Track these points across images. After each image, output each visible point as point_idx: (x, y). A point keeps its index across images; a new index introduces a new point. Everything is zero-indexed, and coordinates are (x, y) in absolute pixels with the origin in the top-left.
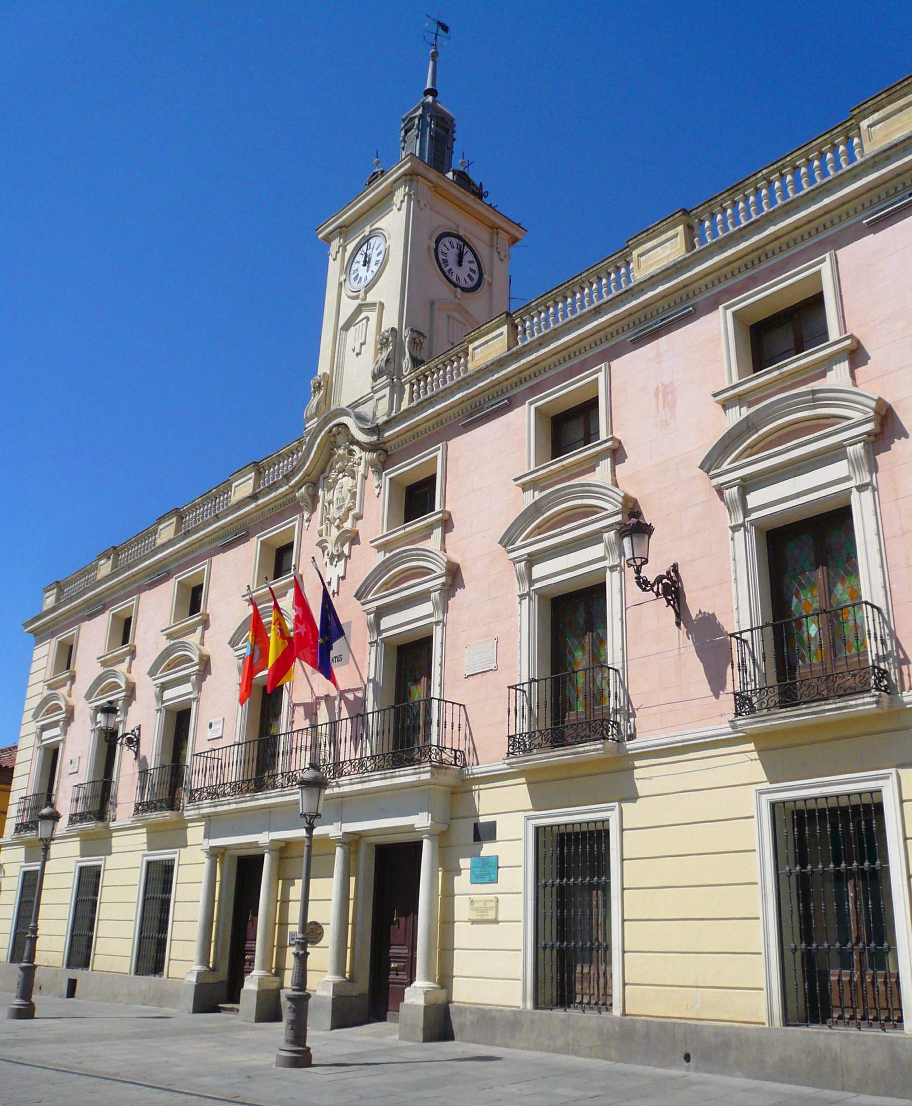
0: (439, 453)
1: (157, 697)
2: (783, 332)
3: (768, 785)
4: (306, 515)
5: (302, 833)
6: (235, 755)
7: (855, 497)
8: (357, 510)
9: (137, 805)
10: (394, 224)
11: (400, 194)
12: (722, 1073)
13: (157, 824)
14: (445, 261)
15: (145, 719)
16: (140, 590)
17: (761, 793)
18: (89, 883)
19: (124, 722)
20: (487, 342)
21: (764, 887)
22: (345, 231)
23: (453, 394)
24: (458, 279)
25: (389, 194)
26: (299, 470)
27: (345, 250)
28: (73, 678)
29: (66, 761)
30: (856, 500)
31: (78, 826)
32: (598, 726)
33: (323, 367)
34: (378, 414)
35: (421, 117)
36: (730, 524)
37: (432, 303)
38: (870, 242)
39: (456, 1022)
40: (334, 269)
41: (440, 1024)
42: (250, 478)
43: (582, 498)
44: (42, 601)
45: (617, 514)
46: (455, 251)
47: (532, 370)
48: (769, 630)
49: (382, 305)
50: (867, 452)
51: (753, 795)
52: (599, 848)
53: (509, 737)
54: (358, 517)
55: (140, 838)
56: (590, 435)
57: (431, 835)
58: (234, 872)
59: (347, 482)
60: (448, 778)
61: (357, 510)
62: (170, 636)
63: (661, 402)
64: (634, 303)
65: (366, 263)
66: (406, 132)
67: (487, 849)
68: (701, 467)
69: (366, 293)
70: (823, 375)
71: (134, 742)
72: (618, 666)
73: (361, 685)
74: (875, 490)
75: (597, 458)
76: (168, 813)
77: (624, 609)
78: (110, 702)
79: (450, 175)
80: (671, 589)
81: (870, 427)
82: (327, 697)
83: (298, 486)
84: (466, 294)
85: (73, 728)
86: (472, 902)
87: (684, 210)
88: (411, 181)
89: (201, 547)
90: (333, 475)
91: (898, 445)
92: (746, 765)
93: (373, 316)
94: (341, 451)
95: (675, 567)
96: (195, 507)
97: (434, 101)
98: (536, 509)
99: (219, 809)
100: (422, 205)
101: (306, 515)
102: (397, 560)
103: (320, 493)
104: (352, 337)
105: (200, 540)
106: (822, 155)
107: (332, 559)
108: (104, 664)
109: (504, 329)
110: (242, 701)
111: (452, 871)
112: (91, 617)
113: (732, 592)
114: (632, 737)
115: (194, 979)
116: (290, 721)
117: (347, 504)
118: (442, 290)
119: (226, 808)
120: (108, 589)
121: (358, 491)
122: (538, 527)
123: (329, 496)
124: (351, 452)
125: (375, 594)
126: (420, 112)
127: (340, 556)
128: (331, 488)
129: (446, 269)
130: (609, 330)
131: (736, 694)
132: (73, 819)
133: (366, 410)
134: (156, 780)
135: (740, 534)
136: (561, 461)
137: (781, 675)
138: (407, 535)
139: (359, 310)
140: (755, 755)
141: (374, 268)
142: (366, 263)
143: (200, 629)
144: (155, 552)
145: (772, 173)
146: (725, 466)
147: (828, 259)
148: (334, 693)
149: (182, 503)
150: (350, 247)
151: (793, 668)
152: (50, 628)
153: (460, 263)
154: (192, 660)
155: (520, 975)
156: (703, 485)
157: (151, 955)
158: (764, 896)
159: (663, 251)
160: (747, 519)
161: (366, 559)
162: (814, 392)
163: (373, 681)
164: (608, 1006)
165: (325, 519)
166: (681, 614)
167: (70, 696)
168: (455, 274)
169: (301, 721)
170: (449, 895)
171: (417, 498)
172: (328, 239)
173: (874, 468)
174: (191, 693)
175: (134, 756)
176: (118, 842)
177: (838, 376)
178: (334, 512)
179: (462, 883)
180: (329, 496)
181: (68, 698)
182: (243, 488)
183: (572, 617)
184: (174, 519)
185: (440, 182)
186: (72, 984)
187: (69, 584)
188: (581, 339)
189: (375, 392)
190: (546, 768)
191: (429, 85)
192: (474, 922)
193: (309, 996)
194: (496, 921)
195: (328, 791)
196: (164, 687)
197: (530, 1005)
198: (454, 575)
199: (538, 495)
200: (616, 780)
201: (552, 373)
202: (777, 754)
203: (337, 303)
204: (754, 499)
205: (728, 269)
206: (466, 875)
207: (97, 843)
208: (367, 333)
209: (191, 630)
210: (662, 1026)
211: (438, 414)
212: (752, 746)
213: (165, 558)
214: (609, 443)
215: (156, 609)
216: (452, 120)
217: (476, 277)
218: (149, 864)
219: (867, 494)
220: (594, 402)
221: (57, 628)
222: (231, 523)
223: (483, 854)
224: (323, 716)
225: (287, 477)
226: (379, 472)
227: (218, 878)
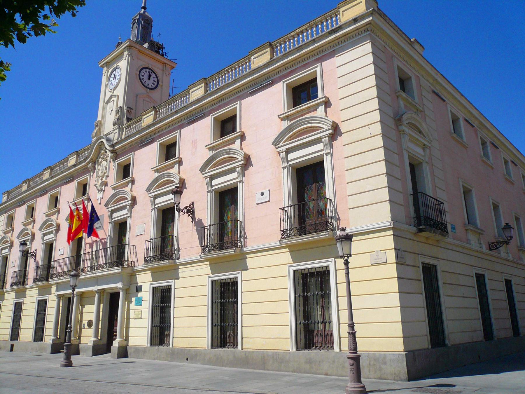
0: (178, 134)
1: (109, 216)
2: (303, 93)
3: (211, 275)
4: (92, 174)
5: (71, 291)
6: (67, 261)
8: (107, 174)
9: (34, 279)
10: (123, 64)
11: (126, 53)
12: (195, 363)
13: (42, 286)
14: (143, 79)
15: (37, 247)
16: (37, 197)
17: (209, 277)
18: (42, 306)
19: (31, 248)
21: (208, 307)
22: (108, 64)
23: (135, 136)
24: (148, 85)
25: (122, 53)
26: (89, 157)
27: (108, 72)
28: (13, 230)
29: (10, 262)
31: (14, 287)
32: (324, 225)
33: (99, 118)
34: (115, 139)
35: (138, 19)
37: (137, 96)
38: (250, 98)
39: (129, 351)
40: (104, 78)
41: (123, 353)
42: (202, 87)
43: (312, 123)
44: (2, 199)
46: (148, 74)
47: (311, 54)
48: (297, 207)
49: (118, 96)
50: (329, 141)
51: (149, 285)
52: (235, 288)
53: (281, 231)
54: (107, 176)
55: (36, 291)
56: (234, 130)
57: (123, 290)
58: (109, 299)
59: (104, 163)
60: (129, 270)
61: (107, 174)
62: (47, 216)
64: (187, 111)
65: (114, 78)
66: (133, 24)
67: (140, 294)
69: (114, 90)
71: (34, 255)
72: (241, 220)
75: (235, 139)
76: (44, 282)
78: (24, 241)
79: (146, 45)
81: (330, 131)
82: (96, 241)
83: (89, 163)
84: (152, 91)
85: (13, 249)
87: (204, 78)
88: (130, 49)
89: (58, 182)
90: (100, 160)
92: (286, 256)
93: (115, 99)
94: (103, 151)
95: (193, 204)
96: (56, 166)
97: (144, 12)
98: (289, 129)
99: (60, 281)
100: (134, 58)
103: (96, 166)
104: (109, 107)
105: (57, 180)
106: (332, 18)
107: (99, 191)
108: (24, 225)
109: (153, 112)
110: (68, 241)
111: (130, 302)
112: (20, 206)
113: (206, 213)
114: (179, 258)
115: (51, 342)
116: (85, 249)
117: (104, 171)
118: (141, 90)
119: (62, 281)
120: (25, 196)
121: (108, 166)
122: (290, 137)
123: (99, 168)
124: (106, 152)
125: (154, 189)
126: (138, 17)
127: (101, 190)
128: (99, 164)
129: (143, 82)
130: (215, 101)
131: (281, 231)
132: (12, 285)
133: (111, 136)
134: (212, 232)
135: (286, 170)
136: (300, 107)
137: (300, 224)
138: (223, 143)
139: (111, 96)
140: (209, 266)
141: (117, 81)
142: (114, 78)
143: (57, 213)
144: (41, 183)
145: (229, 69)
146: (206, 171)
148: (98, 240)
149: (52, 164)
150: (110, 71)
151: (304, 221)
152: (4, 209)
153: (149, 79)
154: (127, 199)
155: (146, 336)
156: (201, 176)
157: (39, 335)
158: (208, 309)
159: (260, 59)
161: (109, 192)
162: (229, 149)
163: (110, 236)
164: (332, 348)
165: (97, 176)
166: (193, 219)
167: (58, 219)
168: (146, 85)
169: (88, 250)
170: (129, 310)
171: (125, 171)
172: (102, 67)
173: (332, 147)
174: (127, 214)
176: (28, 293)
177: (321, 110)
178: (100, 174)
179: (132, 305)
180: (99, 168)
181: (32, 230)
182: (72, 161)
183: (166, 216)
184: (49, 170)
185: (141, 49)
186: (12, 346)
187: (12, 192)
188: (173, 121)
189: (114, 130)
190: (294, 245)
191: (143, 5)
192: (135, 319)
194: (141, 318)
195: (80, 277)
196: (44, 235)
197: (149, 345)
198: (134, 200)
199: (289, 123)
200: (173, 273)
201: (278, 76)
202: (297, 253)
203: (105, 93)
205: (284, 67)
206: (134, 303)
207: (21, 294)
208: (112, 107)
209: (54, 214)
210: (182, 349)
211: (132, 142)
213: (45, 186)
214: (324, 99)
215: (42, 204)
216: (151, 19)
217: (156, 83)
218: (39, 301)
219: (329, 157)
220: (235, 116)
221: (27, 201)
222: (67, 174)
223: (139, 296)
225: (85, 160)
226: (114, 161)
227: (61, 305)
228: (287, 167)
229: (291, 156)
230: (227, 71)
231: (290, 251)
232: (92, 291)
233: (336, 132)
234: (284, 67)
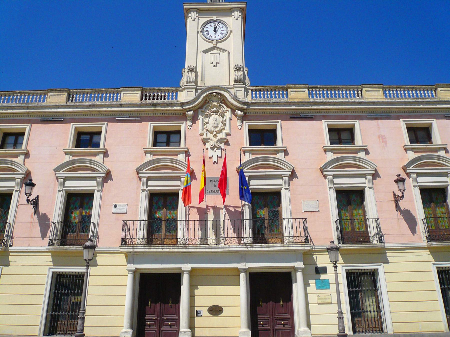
2: (86, 140)
3: (52, 267)
7: (14, 192)
20: (297, 91)
30: (96, 192)
36: (58, 189)
38: (40, 125)
43: (174, 163)
45: (290, 172)
50: (21, 182)
51: (48, 269)
63: (381, 140)
67: (323, 277)
68: (54, 170)
70: (177, 155)
72: (96, 222)
73: (241, 206)
74: (101, 192)
77: (18, 206)
80: (35, 203)
86: (318, 296)
91: (110, 182)
92: (48, 259)
101: (189, 123)
111: (306, 284)
113: (54, 209)
114: (11, 246)
125: (63, 171)
136: (264, 147)
145: (410, 88)
146: (61, 172)
148: (220, 204)
155: (39, 324)
173: (103, 186)
175: (33, 210)
192: (318, 304)
193: (84, 335)
194: (331, 303)
212: (124, 255)
214: (26, 151)
219: (99, 193)
228: (62, 190)
229: (67, 183)
230: (404, 88)
231: (52, 256)
232: (237, 269)
233: (108, 176)
234: (108, 113)
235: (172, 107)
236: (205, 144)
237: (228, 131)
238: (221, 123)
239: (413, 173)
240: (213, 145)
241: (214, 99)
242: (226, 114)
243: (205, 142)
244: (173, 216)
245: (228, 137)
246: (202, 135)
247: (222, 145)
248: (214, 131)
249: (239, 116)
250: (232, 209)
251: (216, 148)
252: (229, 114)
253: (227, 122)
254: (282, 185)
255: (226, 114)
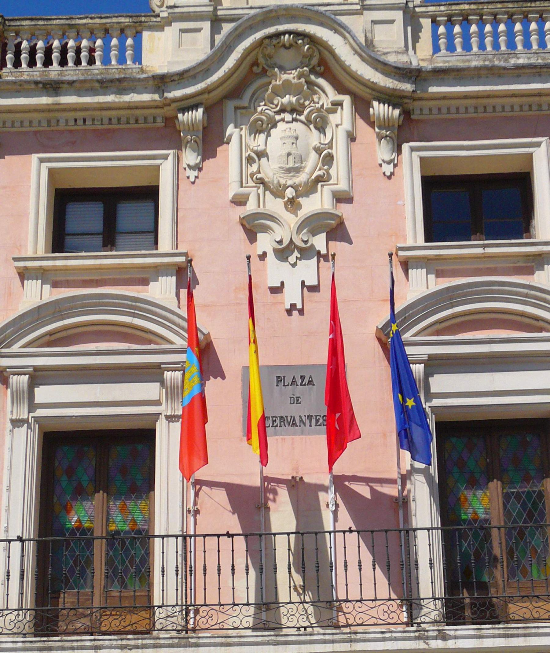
43: (134, 315)
70: (145, 282)
73: (395, 475)
83: (188, 104)
101: (190, 157)
102: (493, 292)
147: (171, 158)
160: (31, 415)
204: (43, 394)
224: (282, 517)
235: (121, 91)
236: (252, 236)
237: (343, 186)
238: (313, 156)
239: (19, 371)
240: (286, 242)
241: (285, 56)
242: (334, 119)
243: (252, 228)
244: (134, 521)
245: (344, 210)
246: (240, 201)
247: (319, 242)
248: (286, 187)
249: (385, 124)
250: (364, 491)
251: (296, 254)
252: (343, 119)
253: (340, 151)
254: (157, 403)
255: (334, 119)
